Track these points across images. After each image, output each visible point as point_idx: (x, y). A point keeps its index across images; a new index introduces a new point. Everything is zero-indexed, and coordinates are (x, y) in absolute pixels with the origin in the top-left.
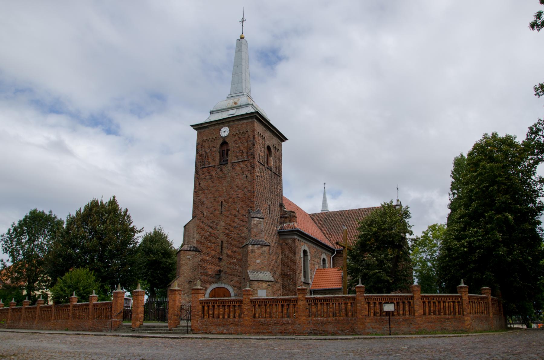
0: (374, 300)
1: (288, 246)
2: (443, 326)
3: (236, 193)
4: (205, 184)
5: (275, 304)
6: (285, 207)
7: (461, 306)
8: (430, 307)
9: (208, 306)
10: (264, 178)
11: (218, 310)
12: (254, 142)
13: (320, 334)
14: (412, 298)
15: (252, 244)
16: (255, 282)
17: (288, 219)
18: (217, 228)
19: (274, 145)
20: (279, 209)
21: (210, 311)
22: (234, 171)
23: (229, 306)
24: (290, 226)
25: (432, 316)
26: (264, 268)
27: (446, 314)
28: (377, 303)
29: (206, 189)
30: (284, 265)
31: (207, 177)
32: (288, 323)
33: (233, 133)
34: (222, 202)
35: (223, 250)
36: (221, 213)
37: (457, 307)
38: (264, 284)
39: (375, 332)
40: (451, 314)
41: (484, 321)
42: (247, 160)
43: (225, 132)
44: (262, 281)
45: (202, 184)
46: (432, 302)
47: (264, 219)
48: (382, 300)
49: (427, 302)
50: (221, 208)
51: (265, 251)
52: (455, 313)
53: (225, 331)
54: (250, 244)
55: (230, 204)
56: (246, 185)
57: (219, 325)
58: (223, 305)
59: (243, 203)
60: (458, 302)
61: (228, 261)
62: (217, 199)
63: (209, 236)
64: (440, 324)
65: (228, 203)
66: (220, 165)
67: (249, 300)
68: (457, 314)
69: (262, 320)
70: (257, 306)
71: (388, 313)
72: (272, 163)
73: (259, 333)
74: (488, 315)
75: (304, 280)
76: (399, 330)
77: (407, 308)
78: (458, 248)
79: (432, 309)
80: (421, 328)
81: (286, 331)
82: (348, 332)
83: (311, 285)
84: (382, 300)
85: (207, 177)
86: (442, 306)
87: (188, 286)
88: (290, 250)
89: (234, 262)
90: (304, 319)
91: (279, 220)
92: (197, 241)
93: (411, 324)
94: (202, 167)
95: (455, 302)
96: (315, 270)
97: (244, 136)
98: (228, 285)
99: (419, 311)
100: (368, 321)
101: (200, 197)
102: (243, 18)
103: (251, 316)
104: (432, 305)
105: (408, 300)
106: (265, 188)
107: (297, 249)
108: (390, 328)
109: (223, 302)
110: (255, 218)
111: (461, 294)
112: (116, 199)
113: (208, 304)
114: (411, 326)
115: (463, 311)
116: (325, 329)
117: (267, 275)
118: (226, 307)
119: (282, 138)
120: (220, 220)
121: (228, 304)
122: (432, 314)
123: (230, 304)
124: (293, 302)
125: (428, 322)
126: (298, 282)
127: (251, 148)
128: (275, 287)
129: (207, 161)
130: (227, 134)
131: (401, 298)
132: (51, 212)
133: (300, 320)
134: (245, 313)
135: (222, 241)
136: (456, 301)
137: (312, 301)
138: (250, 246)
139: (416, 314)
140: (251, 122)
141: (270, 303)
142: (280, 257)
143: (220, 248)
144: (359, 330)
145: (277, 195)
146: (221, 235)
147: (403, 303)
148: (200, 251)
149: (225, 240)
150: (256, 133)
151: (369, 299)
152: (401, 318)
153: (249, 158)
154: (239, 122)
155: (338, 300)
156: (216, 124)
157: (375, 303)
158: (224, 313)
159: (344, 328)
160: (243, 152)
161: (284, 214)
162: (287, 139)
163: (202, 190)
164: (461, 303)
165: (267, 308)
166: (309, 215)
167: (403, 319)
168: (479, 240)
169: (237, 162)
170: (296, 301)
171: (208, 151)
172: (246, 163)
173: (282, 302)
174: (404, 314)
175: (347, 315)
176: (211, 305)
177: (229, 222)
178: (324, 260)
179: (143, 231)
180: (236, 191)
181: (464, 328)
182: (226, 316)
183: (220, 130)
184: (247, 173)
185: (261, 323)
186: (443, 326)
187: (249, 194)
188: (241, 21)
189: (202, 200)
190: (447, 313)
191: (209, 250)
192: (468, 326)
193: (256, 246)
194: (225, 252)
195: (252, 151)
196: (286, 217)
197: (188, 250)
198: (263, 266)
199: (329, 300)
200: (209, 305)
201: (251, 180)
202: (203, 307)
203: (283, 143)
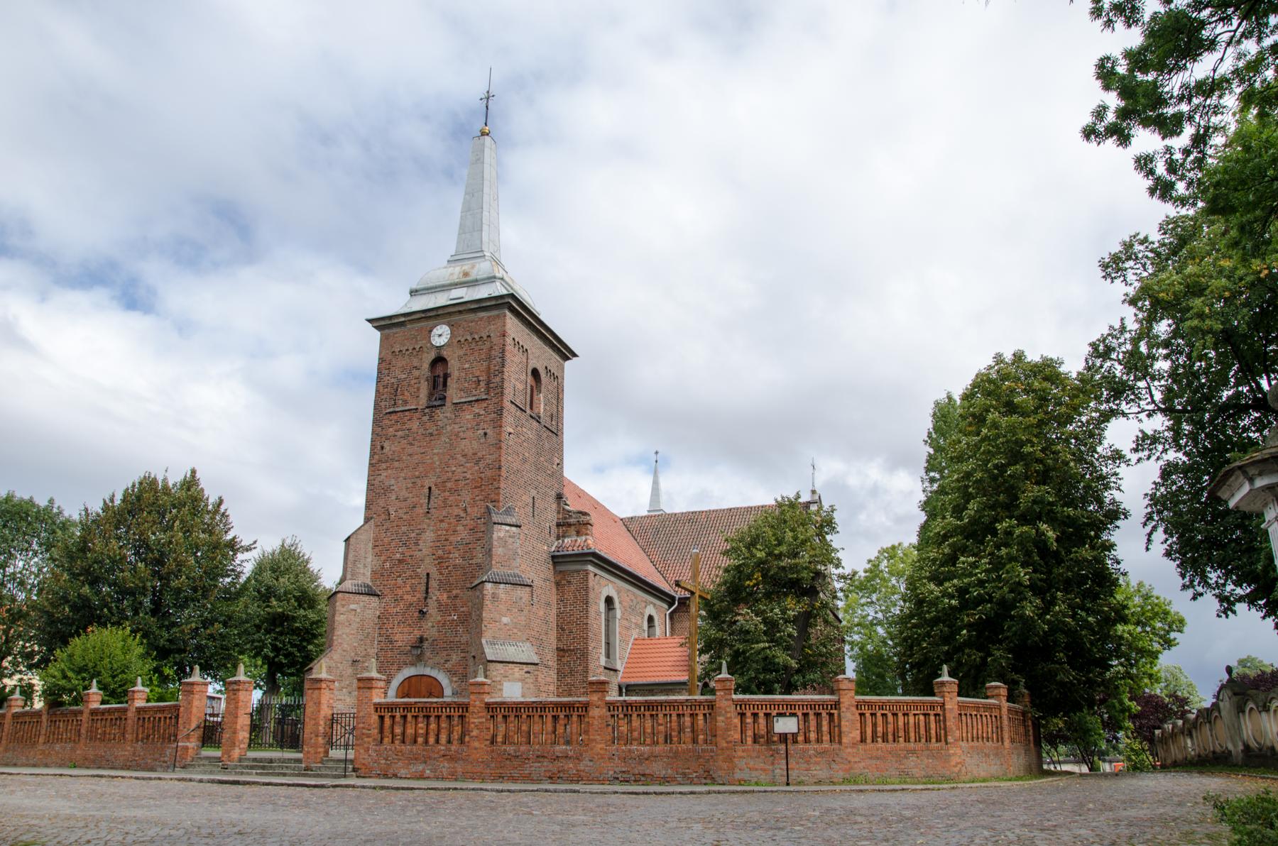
1: (573, 588)
3: (460, 470)
4: (393, 448)
5: (539, 713)
6: (568, 502)
7: (942, 723)
8: (875, 725)
9: (393, 717)
11: (414, 726)
12: (503, 358)
13: (635, 781)
14: (837, 705)
15: (493, 582)
17: (573, 528)
18: (417, 544)
19: (546, 368)
20: (554, 506)
21: (396, 727)
22: (458, 420)
23: (438, 717)
24: (577, 545)
25: (880, 744)
26: (519, 634)
27: (909, 741)
28: (761, 715)
29: (396, 459)
30: (563, 629)
31: (400, 433)
32: (567, 757)
33: (459, 338)
34: (430, 488)
35: (431, 594)
36: (428, 512)
37: (933, 725)
38: (517, 669)
39: (756, 780)
40: (920, 741)
41: (992, 757)
42: (487, 399)
43: (441, 335)
44: (513, 663)
45: (388, 448)
46: (879, 715)
47: (520, 527)
49: (868, 715)
50: (429, 501)
51: (521, 598)
52: (928, 740)
53: (428, 772)
54: (489, 582)
55: (447, 494)
56: (484, 453)
57: (416, 759)
59: (477, 491)
60: (935, 715)
61: (439, 618)
63: (400, 561)
64: (896, 762)
65: (445, 491)
66: (427, 407)
67: (483, 705)
68: (934, 740)
69: (510, 749)
70: (500, 718)
71: (784, 738)
72: (542, 406)
73: (503, 777)
74: (1000, 743)
75: (606, 662)
76: (807, 775)
77: (825, 728)
78: (937, 598)
79: (880, 729)
81: (561, 775)
82: (696, 777)
83: (620, 674)
86: (901, 723)
87: (350, 671)
88: (575, 597)
89: (453, 620)
90: (601, 749)
91: (554, 529)
92: (374, 572)
93: (834, 761)
94: (388, 411)
95: (929, 714)
96: (632, 640)
97: (482, 347)
100: (740, 753)
101: (382, 477)
102: (488, 92)
103: (487, 740)
105: (827, 709)
106: (525, 461)
107: (592, 595)
110: (502, 524)
111: (943, 697)
112: (198, 476)
113: (392, 711)
114: (834, 765)
115: (946, 736)
116: (647, 772)
118: (432, 719)
119: (565, 352)
120: (425, 526)
121: (436, 714)
122: (879, 739)
123: (440, 713)
125: (871, 758)
126: (591, 666)
127: (497, 373)
129: (401, 397)
130: (446, 341)
131: (811, 705)
132: (51, 501)
133: (592, 749)
134: (472, 734)
135: (428, 574)
136: (932, 713)
137: (620, 709)
138: (489, 586)
139: (845, 740)
140: (498, 316)
143: (424, 588)
144: (720, 773)
145: (551, 476)
146: (427, 561)
147: (818, 715)
148: (378, 596)
149: (434, 572)
150: (509, 341)
151: (743, 706)
152: (812, 747)
154: (471, 316)
157: (755, 715)
158: (427, 733)
159: (689, 768)
160: (479, 381)
161: (565, 518)
163: (387, 462)
164: (941, 718)
165: (522, 723)
166: (622, 520)
167: (815, 750)
168: (981, 583)
169: (465, 402)
171: (404, 376)
172: (485, 405)
174: (819, 741)
175: (695, 741)
177: (444, 532)
178: (651, 619)
179: (255, 548)
182: (432, 740)
183: (431, 331)
184: (486, 426)
185: (506, 756)
187: (489, 473)
188: (483, 97)
189: (387, 484)
190: (912, 739)
191: (400, 592)
192: (955, 766)
193: (502, 586)
194: (435, 598)
195: (498, 379)
196: (569, 525)
197: (352, 593)
198: (515, 631)
200: (394, 714)
201: (494, 442)
202: (382, 718)
203: (567, 363)
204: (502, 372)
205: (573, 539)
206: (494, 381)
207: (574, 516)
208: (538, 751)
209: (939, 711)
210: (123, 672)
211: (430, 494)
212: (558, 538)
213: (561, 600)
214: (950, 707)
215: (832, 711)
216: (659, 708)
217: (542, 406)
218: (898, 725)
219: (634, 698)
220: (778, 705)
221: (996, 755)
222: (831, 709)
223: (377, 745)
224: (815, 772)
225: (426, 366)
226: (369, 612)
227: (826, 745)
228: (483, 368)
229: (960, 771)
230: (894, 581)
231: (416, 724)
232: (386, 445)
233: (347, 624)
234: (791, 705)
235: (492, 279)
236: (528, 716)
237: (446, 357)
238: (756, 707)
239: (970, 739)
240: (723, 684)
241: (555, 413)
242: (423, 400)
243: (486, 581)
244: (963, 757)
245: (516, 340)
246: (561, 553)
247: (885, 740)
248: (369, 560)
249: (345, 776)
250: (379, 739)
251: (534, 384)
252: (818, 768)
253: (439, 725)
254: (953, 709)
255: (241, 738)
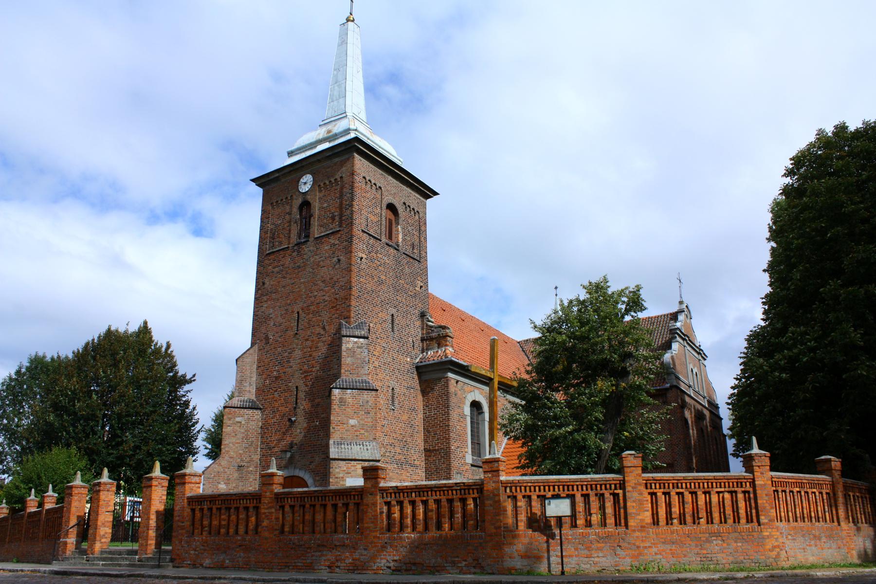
0: (526, 491)
2: (705, 552)
8: (669, 505)
9: (202, 510)
10: (379, 263)
11: (218, 518)
12: (352, 194)
13: (406, 570)
14: (622, 485)
15: (340, 388)
16: (340, 462)
17: (434, 341)
18: (288, 362)
19: (404, 203)
20: (418, 323)
23: (237, 509)
26: (366, 434)
27: (712, 523)
30: (429, 432)
34: (298, 313)
35: (299, 404)
36: (296, 333)
37: (742, 504)
40: (725, 522)
41: (824, 539)
42: (340, 230)
44: (355, 460)
45: (268, 283)
46: (673, 493)
48: (544, 490)
51: (367, 402)
52: (737, 519)
53: (227, 561)
54: (336, 388)
56: (338, 277)
57: (218, 549)
58: (226, 506)
59: (333, 311)
60: (744, 492)
62: (290, 308)
63: (277, 378)
64: (697, 546)
67: (273, 496)
68: (743, 520)
70: (287, 509)
72: (400, 236)
74: (836, 523)
76: (588, 563)
77: (609, 510)
78: (766, 372)
79: (675, 510)
80: (646, 557)
81: (339, 564)
84: (544, 490)
85: (276, 269)
87: (236, 475)
88: (438, 402)
89: (316, 426)
91: (418, 343)
92: (258, 389)
93: (620, 546)
94: (268, 252)
95: (736, 492)
98: (305, 471)
99: (639, 515)
101: (264, 308)
103: (276, 530)
104: (675, 499)
105: (611, 488)
106: (381, 283)
107: (453, 400)
108: (562, 556)
109: (228, 500)
112: (149, 326)
113: (201, 504)
116: (418, 560)
117: (369, 448)
118: (232, 510)
119: (427, 192)
121: (235, 505)
122: (675, 521)
123: (238, 505)
124: (354, 499)
125: (664, 543)
126: (455, 463)
127: (347, 207)
128: (408, 474)
130: (310, 187)
135: (297, 387)
136: (739, 490)
137: (393, 495)
139: (631, 523)
141: (311, 500)
142: (421, 416)
149: (301, 384)
150: (358, 179)
151: (514, 488)
153: (344, 226)
155: (446, 492)
156: (291, 171)
158: (229, 525)
159: (458, 557)
161: (429, 333)
162: (436, 194)
164: (752, 495)
166: (519, 343)
168: (813, 350)
169: (324, 236)
170: (360, 496)
171: (280, 222)
172: (339, 235)
173: (334, 497)
174: (604, 524)
176: (206, 507)
180: (322, 290)
181: (764, 557)
182: (232, 531)
186: (705, 552)
187: (342, 294)
192: (771, 550)
193: (349, 391)
194: (302, 407)
195: (348, 212)
196: (431, 339)
197: (237, 408)
198: (362, 432)
199: (427, 492)
202: (193, 510)
203: (429, 201)
204: (352, 206)
205: (435, 351)
206: (345, 214)
207: (435, 330)
208: (319, 540)
209: (748, 488)
210: (62, 482)
211: (298, 318)
212: (423, 352)
213: (426, 406)
214: (762, 483)
215: (615, 491)
216: (430, 493)
217: (400, 236)
218: (697, 505)
219: (433, 482)
220: (554, 486)
221: (830, 537)
222: (616, 488)
223: (188, 537)
224: (596, 559)
225: (295, 210)
226: (253, 423)
227: (611, 528)
228: (337, 205)
229: (778, 556)
230: (758, 372)
231: (220, 516)
232: (267, 281)
233: (233, 434)
234: (568, 486)
235: (347, 131)
236: (311, 505)
237: (310, 200)
238: (528, 488)
239: (791, 519)
240: (490, 465)
241: (416, 243)
242: (294, 239)
243: (333, 388)
244: (781, 540)
245: (368, 178)
246: (424, 364)
247: (682, 521)
248: (254, 379)
249: (159, 566)
250: (191, 531)
251: (392, 217)
252: (601, 554)
253: (238, 516)
254: (765, 485)
255: (102, 533)
